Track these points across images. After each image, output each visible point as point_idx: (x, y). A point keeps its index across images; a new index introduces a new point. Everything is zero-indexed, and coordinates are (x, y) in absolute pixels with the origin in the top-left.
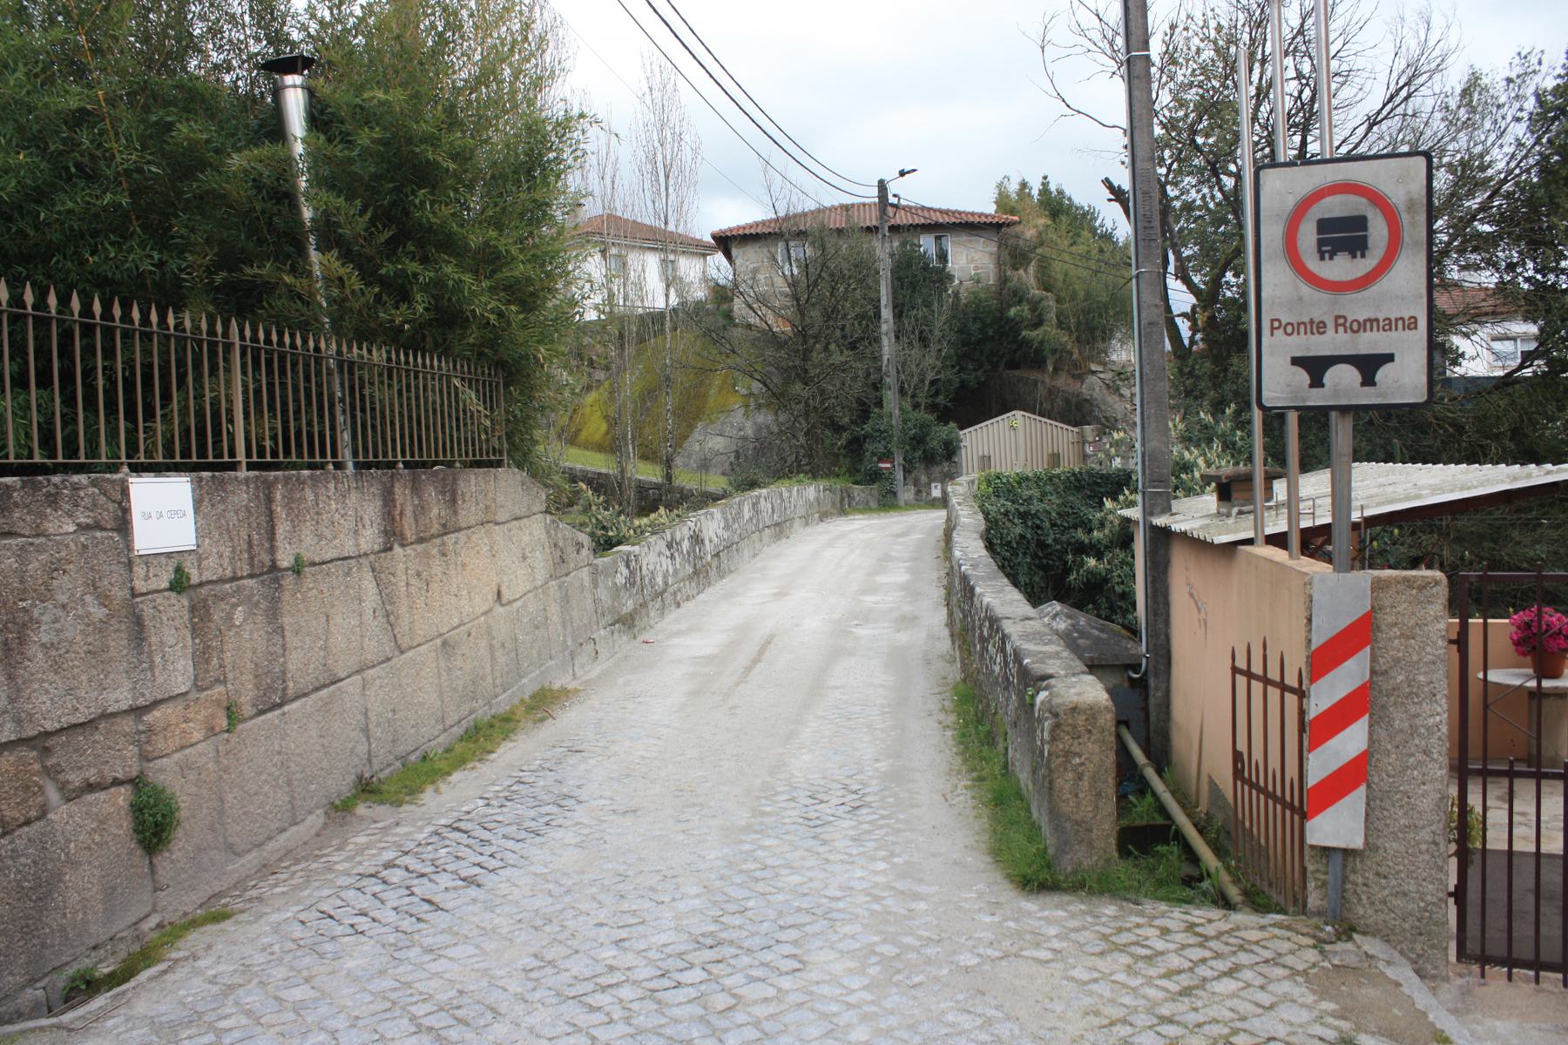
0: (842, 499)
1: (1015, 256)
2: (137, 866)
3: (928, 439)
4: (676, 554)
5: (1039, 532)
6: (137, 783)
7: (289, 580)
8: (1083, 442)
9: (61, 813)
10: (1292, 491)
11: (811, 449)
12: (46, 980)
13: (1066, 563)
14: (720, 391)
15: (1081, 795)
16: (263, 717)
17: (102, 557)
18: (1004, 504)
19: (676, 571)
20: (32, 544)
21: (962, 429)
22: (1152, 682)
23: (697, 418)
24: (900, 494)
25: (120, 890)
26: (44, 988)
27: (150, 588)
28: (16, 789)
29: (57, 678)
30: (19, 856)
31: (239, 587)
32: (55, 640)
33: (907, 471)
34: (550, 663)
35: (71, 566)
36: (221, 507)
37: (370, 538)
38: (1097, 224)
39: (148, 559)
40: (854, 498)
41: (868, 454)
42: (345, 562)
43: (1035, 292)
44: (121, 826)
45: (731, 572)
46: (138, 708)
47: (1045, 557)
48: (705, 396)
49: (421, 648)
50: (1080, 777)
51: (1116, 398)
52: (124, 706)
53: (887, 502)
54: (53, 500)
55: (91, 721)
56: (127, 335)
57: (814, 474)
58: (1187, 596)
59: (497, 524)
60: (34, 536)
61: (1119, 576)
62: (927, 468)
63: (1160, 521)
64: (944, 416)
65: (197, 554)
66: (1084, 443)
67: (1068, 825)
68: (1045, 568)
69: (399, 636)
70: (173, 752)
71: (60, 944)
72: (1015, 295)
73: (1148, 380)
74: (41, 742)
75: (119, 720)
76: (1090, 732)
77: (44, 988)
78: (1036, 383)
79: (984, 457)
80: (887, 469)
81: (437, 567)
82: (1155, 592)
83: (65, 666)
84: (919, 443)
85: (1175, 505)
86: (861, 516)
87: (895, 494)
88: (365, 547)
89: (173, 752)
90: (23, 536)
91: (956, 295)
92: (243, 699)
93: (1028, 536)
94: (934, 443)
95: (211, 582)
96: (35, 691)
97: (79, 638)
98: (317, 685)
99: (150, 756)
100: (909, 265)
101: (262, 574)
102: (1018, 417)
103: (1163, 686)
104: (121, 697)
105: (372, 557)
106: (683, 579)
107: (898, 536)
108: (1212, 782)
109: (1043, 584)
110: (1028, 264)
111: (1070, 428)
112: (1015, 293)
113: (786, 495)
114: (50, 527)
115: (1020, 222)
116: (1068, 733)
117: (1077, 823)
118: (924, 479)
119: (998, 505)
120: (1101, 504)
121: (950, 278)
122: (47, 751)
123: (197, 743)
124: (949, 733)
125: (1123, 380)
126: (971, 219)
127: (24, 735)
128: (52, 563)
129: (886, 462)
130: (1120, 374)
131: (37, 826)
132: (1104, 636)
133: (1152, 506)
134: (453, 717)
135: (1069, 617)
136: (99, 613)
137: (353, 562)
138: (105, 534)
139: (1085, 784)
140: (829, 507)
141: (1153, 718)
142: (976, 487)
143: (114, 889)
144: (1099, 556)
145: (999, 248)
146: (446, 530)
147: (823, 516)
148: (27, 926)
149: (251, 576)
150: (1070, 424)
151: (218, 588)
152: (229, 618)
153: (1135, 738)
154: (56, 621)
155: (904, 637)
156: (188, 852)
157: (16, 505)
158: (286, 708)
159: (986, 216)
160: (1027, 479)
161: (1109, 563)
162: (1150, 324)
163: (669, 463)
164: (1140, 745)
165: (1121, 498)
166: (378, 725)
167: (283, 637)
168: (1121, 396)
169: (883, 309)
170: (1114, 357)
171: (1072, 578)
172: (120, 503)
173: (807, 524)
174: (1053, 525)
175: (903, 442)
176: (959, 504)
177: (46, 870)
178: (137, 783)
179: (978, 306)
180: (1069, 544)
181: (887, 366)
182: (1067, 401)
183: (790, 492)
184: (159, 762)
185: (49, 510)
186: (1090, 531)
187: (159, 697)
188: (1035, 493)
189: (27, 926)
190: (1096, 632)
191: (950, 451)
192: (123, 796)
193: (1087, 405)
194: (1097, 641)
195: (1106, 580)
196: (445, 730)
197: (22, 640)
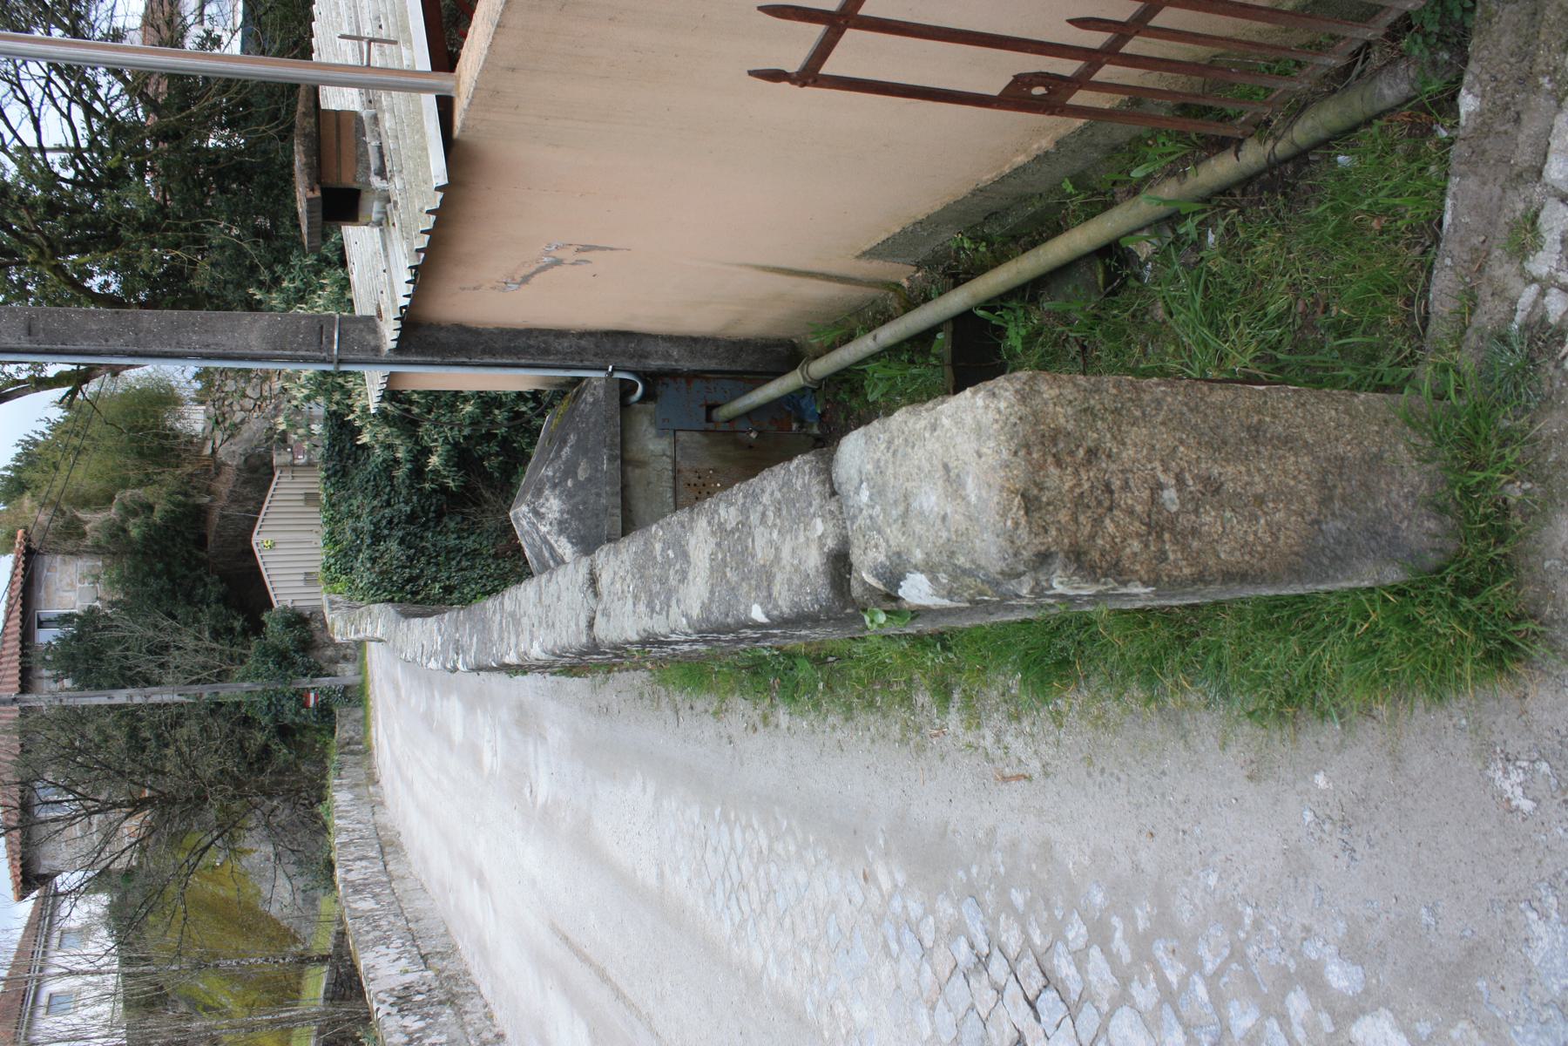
0: (352, 753)
1: (69, 536)
3: (281, 647)
5: (396, 521)
8: (292, 466)
10: (344, 77)
11: (289, 791)
13: (433, 490)
14: (221, 884)
15: (1260, 488)
18: (361, 562)
21: (271, 605)
22: (654, 364)
24: (348, 682)
33: (320, 672)
38: (42, 439)
40: (351, 738)
41: (297, 720)
43: (113, 513)
45: (447, 933)
47: (426, 514)
48: (226, 901)
50: (1213, 487)
51: (245, 427)
53: (356, 696)
57: (319, 793)
58: (525, 287)
61: (451, 429)
62: (317, 648)
63: (389, 333)
64: (257, 627)
66: (294, 465)
67: (1333, 526)
68: (440, 515)
72: (118, 536)
73: (137, 342)
76: (1092, 453)
78: (223, 517)
79: (305, 580)
80: (316, 697)
82: (508, 351)
84: (285, 658)
85: (363, 308)
86: (373, 729)
87: (347, 687)
91: (113, 604)
93: (400, 534)
94: (287, 640)
100: (72, 657)
102: (258, 540)
103: (662, 346)
106: (462, 1027)
107: (398, 696)
108: (871, 254)
109: (459, 518)
110: (79, 520)
111: (275, 480)
112: (113, 536)
113: (343, 838)
115: (26, 528)
116: (1098, 522)
117: (1325, 501)
118: (330, 652)
119: (364, 574)
120: (364, 447)
121: (92, 611)
124: (782, 717)
125: (224, 421)
126: (18, 586)
129: (308, 697)
130: (217, 422)
132: (572, 438)
133: (363, 348)
135: (539, 493)
139: (1230, 473)
140: (362, 771)
141: (712, 365)
142: (339, 598)
144: (427, 452)
145: (56, 552)
147: (372, 780)
150: (271, 481)
153: (734, 398)
155: (555, 734)
159: (16, 567)
160: (331, 533)
161: (436, 440)
162: (29, 332)
163: (304, 960)
164: (745, 392)
165: (358, 423)
168: (243, 422)
169: (112, 702)
170: (199, 427)
171: (452, 484)
173: (382, 804)
174: (388, 504)
175: (284, 677)
176: (357, 631)
179: (128, 580)
180: (411, 486)
181: (188, 696)
182: (246, 482)
183: (340, 830)
186: (396, 461)
188: (349, 524)
190: (566, 451)
191: (300, 621)
193: (252, 460)
194: (580, 449)
195: (456, 445)
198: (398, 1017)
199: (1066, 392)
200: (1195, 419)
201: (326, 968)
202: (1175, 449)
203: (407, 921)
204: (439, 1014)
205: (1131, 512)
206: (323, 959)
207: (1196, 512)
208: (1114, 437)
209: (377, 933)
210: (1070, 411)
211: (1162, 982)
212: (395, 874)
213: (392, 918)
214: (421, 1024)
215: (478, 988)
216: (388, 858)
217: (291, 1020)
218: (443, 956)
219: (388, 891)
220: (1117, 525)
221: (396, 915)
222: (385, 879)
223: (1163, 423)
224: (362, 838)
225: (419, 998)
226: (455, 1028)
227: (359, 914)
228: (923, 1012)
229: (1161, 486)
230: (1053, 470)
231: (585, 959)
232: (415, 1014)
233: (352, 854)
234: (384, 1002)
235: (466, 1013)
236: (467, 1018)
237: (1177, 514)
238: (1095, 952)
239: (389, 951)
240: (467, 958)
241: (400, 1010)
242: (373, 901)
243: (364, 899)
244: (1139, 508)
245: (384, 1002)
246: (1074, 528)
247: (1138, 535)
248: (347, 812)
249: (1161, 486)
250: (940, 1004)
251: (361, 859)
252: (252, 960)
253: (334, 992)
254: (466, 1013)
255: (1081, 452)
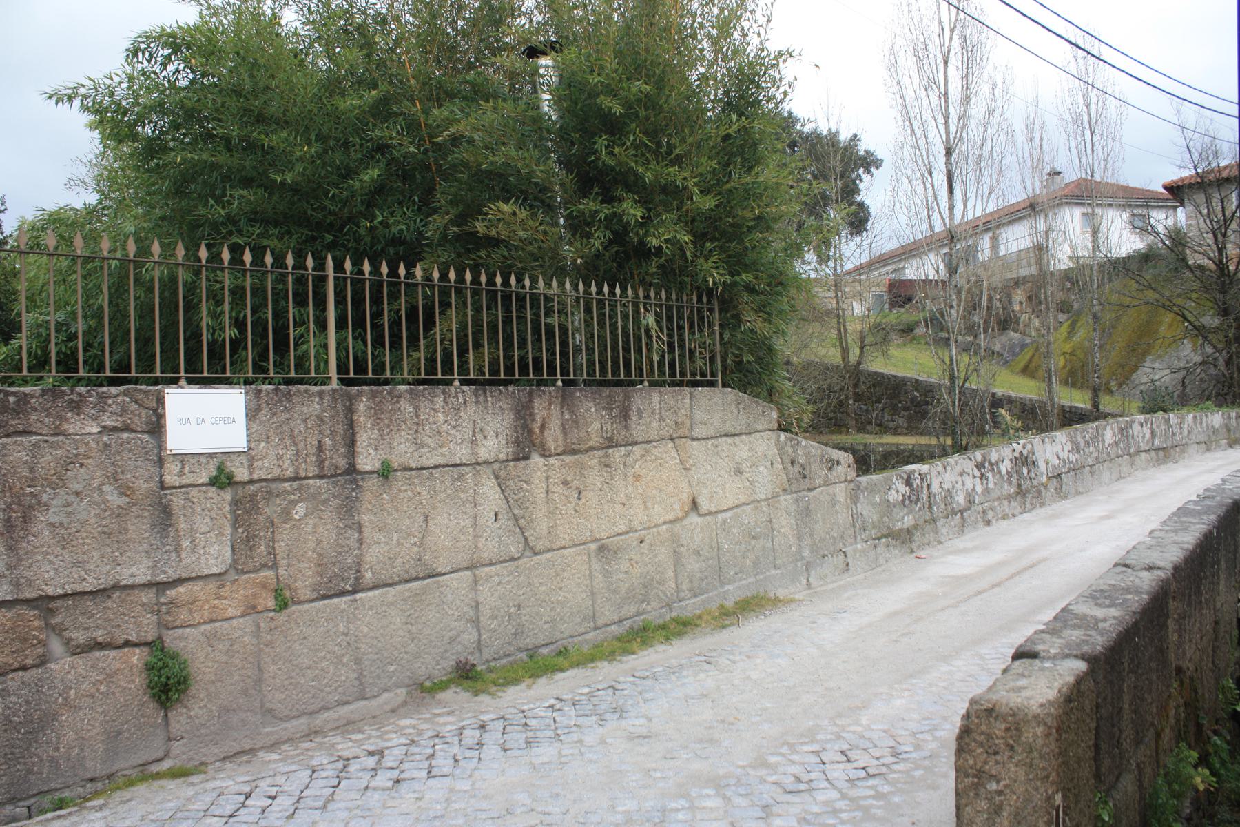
2: (149, 717)
4: (990, 475)
6: (156, 645)
7: (372, 483)
9: (62, 665)
12: (32, 801)
16: (326, 602)
17: (126, 454)
19: (987, 491)
20: (47, 441)
23: (1145, 354)
25: (126, 735)
26: (28, 807)
27: (183, 482)
28: (13, 640)
29: (64, 552)
30: (9, 696)
31: (302, 485)
32: (65, 521)
34: (773, 572)
35: (90, 461)
36: (286, 416)
37: (494, 445)
39: (182, 458)
42: (455, 469)
44: (133, 681)
45: (1078, 493)
46: (158, 584)
49: (565, 552)
50: (998, 810)
52: (141, 580)
54: (77, 407)
55: (104, 590)
56: (475, 293)
59: (693, 439)
60: (52, 435)
65: (249, 456)
69: (530, 539)
70: (199, 624)
71: (48, 773)
74: (44, 604)
75: (136, 592)
77: (28, 807)
81: (595, 477)
83: (74, 543)
88: (483, 454)
89: (199, 624)
90: (41, 435)
92: (299, 584)
95: (265, 480)
96: (38, 561)
97: (92, 521)
98: (406, 577)
99: (170, 625)
101: (336, 475)
104: (140, 572)
105: (496, 466)
114: (71, 428)
116: (981, 745)
122: (52, 612)
123: (232, 618)
127: (21, 596)
128: (68, 458)
131: (33, 672)
134: (609, 614)
136: (115, 499)
137: (466, 469)
138: (133, 435)
143: (119, 733)
146: (611, 443)
148: (12, 753)
149: (321, 477)
151: (273, 486)
152: (286, 514)
154: (68, 505)
156: (211, 711)
157: (35, 410)
158: (358, 596)
166: (493, 617)
167: (360, 532)
172: (155, 410)
173: (1208, 450)
177: (40, 709)
178: (156, 645)
183: (1182, 418)
184: (180, 631)
185: (70, 414)
187: (184, 575)
189: (12, 753)
192: (137, 657)
196: (597, 628)
197: (26, 519)
198: (1011, 457)
199: (1040, 740)
200: (1029, 809)
201: (1089, 407)
202: (1015, 793)
203: (1091, 466)
204: (1010, 483)
205: (986, 762)
206: (1096, 405)
207: (986, 798)
208: (1019, 761)
209: (1082, 445)
210: (1031, 740)
211: (842, 811)
212: (1137, 458)
213: (1095, 455)
214: (1004, 471)
215: (1029, 511)
216: (1153, 453)
217: (1050, 383)
218: (1059, 489)
219: (1120, 452)
220: (980, 754)
221: (1097, 458)
222: (1132, 450)
223: (1027, 790)
224: (1174, 434)
225: (1025, 471)
226: (999, 494)
227: (1100, 431)
228: (885, 727)
229: (998, 782)
230: (1003, 726)
231: (1012, 576)
232: (1012, 468)
233: (1158, 427)
234: (1024, 448)
235: (1010, 502)
236: (1005, 503)
237: (985, 788)
238: (872, 793)
239: (1066, 452)
240: (1054, 506)
241: (1016, 459)
242: (1112, 441)
243: (1114, 434)
244: (987, 767)
245: (1024, 448)
246: (979, 731)
247: (976, 764)
248: (1201, 423)
249: (998, 782)
250: (884, 734)
251: (1152, 433)
252: (1097, 355)
253: (1075, 413)
254: (1010, 502)
255: (1012, 742)
